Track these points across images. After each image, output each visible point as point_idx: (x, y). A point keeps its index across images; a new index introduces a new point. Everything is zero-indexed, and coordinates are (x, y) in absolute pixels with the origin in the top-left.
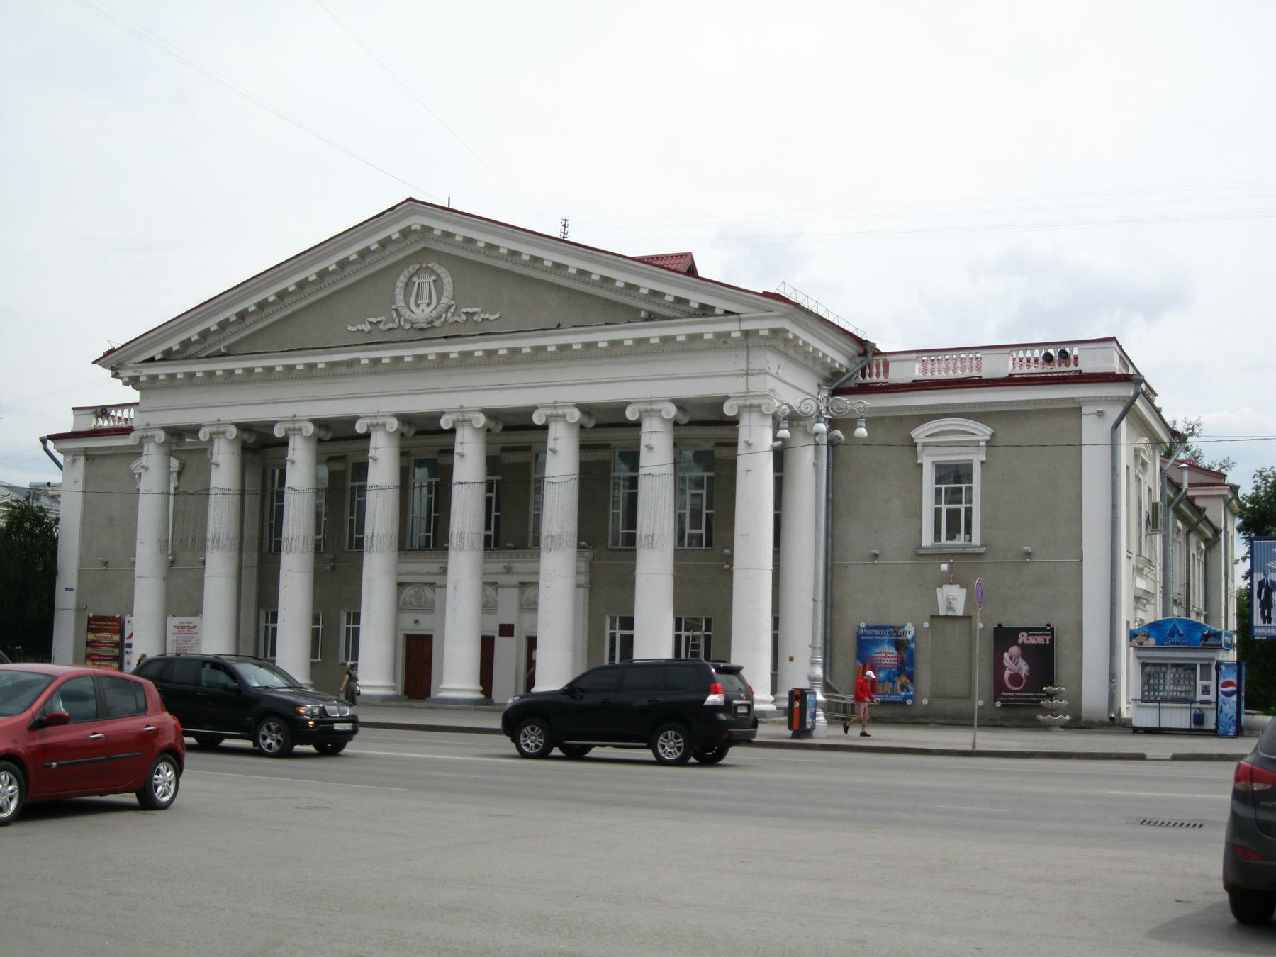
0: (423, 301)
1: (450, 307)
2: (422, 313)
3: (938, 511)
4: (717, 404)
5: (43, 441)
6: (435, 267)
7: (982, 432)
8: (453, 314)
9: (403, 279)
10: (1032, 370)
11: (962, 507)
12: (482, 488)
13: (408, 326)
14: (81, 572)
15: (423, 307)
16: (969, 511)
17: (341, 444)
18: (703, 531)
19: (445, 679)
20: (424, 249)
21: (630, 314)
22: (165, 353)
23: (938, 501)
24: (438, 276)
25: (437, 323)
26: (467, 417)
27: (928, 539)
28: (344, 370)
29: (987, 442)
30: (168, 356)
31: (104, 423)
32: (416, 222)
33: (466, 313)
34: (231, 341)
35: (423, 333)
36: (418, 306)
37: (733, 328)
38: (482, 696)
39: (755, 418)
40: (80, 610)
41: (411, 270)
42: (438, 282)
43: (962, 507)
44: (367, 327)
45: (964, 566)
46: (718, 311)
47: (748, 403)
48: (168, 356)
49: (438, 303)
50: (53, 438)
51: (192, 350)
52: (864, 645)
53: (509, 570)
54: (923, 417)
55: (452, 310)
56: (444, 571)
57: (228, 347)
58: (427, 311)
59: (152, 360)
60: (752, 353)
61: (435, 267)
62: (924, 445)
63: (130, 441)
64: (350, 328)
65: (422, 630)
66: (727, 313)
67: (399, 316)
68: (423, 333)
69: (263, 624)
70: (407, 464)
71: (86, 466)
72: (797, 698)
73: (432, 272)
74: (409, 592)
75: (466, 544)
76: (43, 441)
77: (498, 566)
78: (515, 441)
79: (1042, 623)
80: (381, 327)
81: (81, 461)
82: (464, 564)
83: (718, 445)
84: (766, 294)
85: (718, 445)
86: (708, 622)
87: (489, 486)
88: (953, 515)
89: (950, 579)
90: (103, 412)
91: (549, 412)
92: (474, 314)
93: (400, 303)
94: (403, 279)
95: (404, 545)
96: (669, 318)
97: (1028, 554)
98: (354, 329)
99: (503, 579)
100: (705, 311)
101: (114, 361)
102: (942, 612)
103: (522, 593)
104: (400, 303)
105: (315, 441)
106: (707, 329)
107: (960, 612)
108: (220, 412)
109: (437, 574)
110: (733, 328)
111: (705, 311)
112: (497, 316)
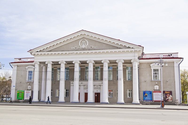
0: (84, 45)
1: (88, 46)
2: (84, 46)
3: (29, 77)
5: (183, 58)
6: (85, 40)
8: (89, 47)
9: (80, 41)
10: (165, 57)
11: (31, 76)
12: (51, 72)
13: (81, 48)
17: (84, 65)
18: (68, 78)
21: (118, 48)
22: (40, 51)
23: (29, 75)
24: (86, 41)
25: (86, 48)
26: (91, 61)
27: (153, 79)
28: (71, 54)
30: (40, 51)
31: (20, 61)
32: (83, 33)
33: (91, 47)
34: (51, 49)
35: (84, 49)
37: (133, 50)
38: (38, 101)
39: (136, 62)
40: (16, 90)
41: (82, 40)
42: (86, 42)
43: (31, 76)
44: (74, 48)
45: (159, 83)
48: (40, 51)
49: (86, 45)
50: (11, 63)
51: (44, 50)
52: (144, 93)
53: (82, 83)
54: (152, 63)
56: (102, 83)
57: (51, 50)
59: (38, 51)
60: (135, 53)
61: (85, 40)
62: (27, 69)
63: (33, 63)
65: (98, 92)
66: (132, 48)
67: (80, 47)
68: (84, 49)
70: (95, 68)
71: (17, 67)
72: (163, 102)
73: (85, 41)
74: (95, 86)
75: (91, 80)
76: (10, 63)
77: (81, 83)
78: (70, 66)
79: (170, 91)
80: (77, 48)
82: (91, 83)
83: (70, 67)
84: (139, 46)
85: (70, 67)
87: (52, 72)
89: (156, 85)
90: (20, 59)
91: (48, 62)
92: (92, 47)
93: (80, 45)
94: (80, 41)
95: (95, 79)
96: (122, 48)
97: (167, 81)
99: (81, 85)
100: (129, 48)
101: (30, 51)
102: (29, 89)
103: (84, 87)
104: (80, 45)
105: (51, 65)
106: (129, 50)
107: (158, 89)
108: (49, 59)
109: (101, 84)
111: (129, 48)
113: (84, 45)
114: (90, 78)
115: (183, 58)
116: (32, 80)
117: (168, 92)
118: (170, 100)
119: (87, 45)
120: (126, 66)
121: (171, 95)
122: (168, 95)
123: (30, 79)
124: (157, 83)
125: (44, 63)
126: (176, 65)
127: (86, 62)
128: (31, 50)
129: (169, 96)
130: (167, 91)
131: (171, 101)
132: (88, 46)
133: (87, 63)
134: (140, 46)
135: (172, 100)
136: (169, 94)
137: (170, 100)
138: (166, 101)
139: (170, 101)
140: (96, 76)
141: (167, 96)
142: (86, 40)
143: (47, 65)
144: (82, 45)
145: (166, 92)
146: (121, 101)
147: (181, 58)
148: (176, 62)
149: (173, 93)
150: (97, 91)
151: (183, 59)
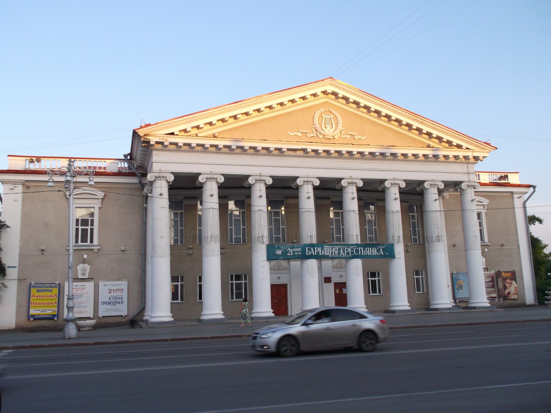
3: (77, 230)
4: (195, 177)
7: (486, 202)
11: (89, 228)
14: (22, 256)
15: (328, 128)
16: (92, 230)
19: (204, 309)
20: (326, 102)
29: (102, 199)
31: (32, 167)
36: (326, 127)
43: (89, 228)
46: (463, 148)
47: (261, 179)
55: (343, 132)
58: (332, 130)
59: (173, 134)
61: (333, 112)
64: (289, 133)
66: (467, 148)
69: (424, 276)
79: (511, 270)
81: (20, 188)
86: (182, 277)
88: (84, 232)
89: (84, 261)
98: (292, 134)
102: (80, 277)
110: (470, 154)
112: (364, 138)
113: (329, 127)
114: (434, 236)
115: (534, 187)
116: (92, 241)
117: (508, 274)
118: (514, 294)
119: (340, 127)
120: (328, 198)
121: (514, 282)
122: (508, 281)
123: (84, 240)
124: (85, 256)
125: (456, 185)
126: (518, 203)
127: (287, 185)
128: (149, 125)
129: (511, 283)
130: (505, 272)
131: (516, 297)
132: (342, 131)
133: (337, 190)
134: (489, 144)
135: (517, 294)
136: (511, 279)
137: (514, 294)
138: (506, 296)
139: (513, 297)
140: (231, 229)
141: (507, 285)
142: (336, 113)
143: (151, 183)
144: (323, 128)
145: (503, 274)
146: (399, 304)
147: (530, 186)
148: (519, 196)
149: (517, 275)
150: (279, 278)
151: (536, 189)
